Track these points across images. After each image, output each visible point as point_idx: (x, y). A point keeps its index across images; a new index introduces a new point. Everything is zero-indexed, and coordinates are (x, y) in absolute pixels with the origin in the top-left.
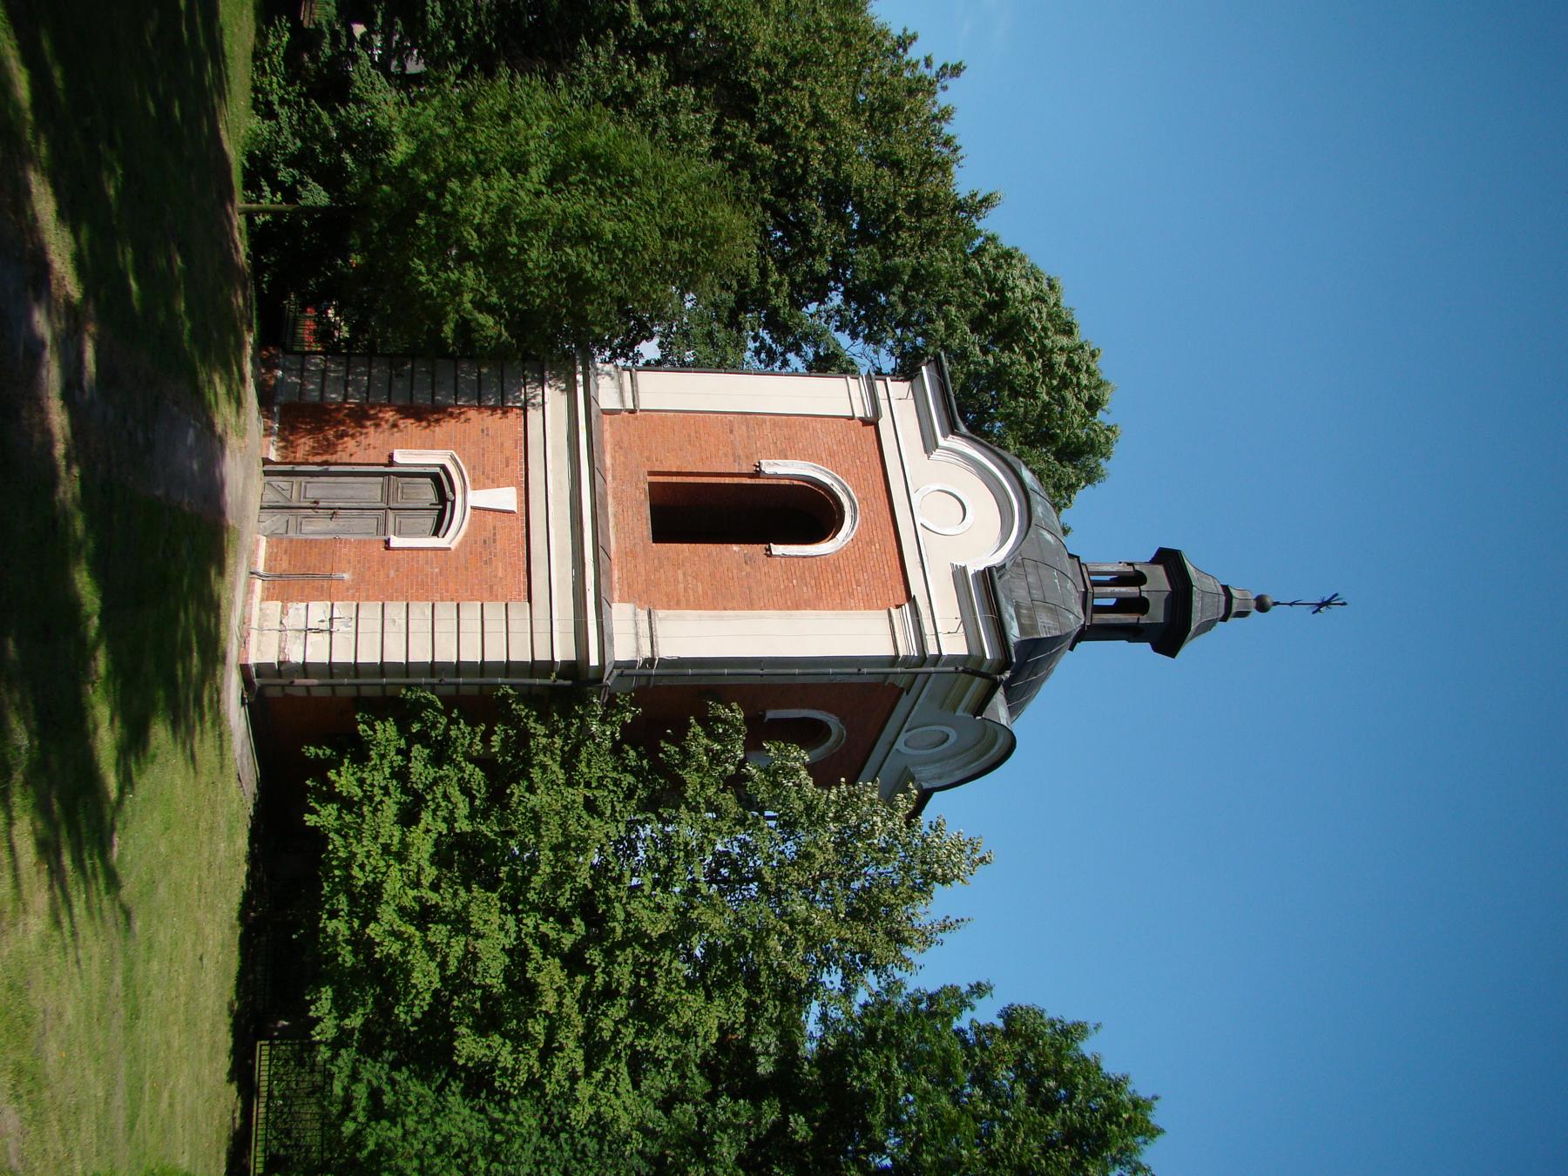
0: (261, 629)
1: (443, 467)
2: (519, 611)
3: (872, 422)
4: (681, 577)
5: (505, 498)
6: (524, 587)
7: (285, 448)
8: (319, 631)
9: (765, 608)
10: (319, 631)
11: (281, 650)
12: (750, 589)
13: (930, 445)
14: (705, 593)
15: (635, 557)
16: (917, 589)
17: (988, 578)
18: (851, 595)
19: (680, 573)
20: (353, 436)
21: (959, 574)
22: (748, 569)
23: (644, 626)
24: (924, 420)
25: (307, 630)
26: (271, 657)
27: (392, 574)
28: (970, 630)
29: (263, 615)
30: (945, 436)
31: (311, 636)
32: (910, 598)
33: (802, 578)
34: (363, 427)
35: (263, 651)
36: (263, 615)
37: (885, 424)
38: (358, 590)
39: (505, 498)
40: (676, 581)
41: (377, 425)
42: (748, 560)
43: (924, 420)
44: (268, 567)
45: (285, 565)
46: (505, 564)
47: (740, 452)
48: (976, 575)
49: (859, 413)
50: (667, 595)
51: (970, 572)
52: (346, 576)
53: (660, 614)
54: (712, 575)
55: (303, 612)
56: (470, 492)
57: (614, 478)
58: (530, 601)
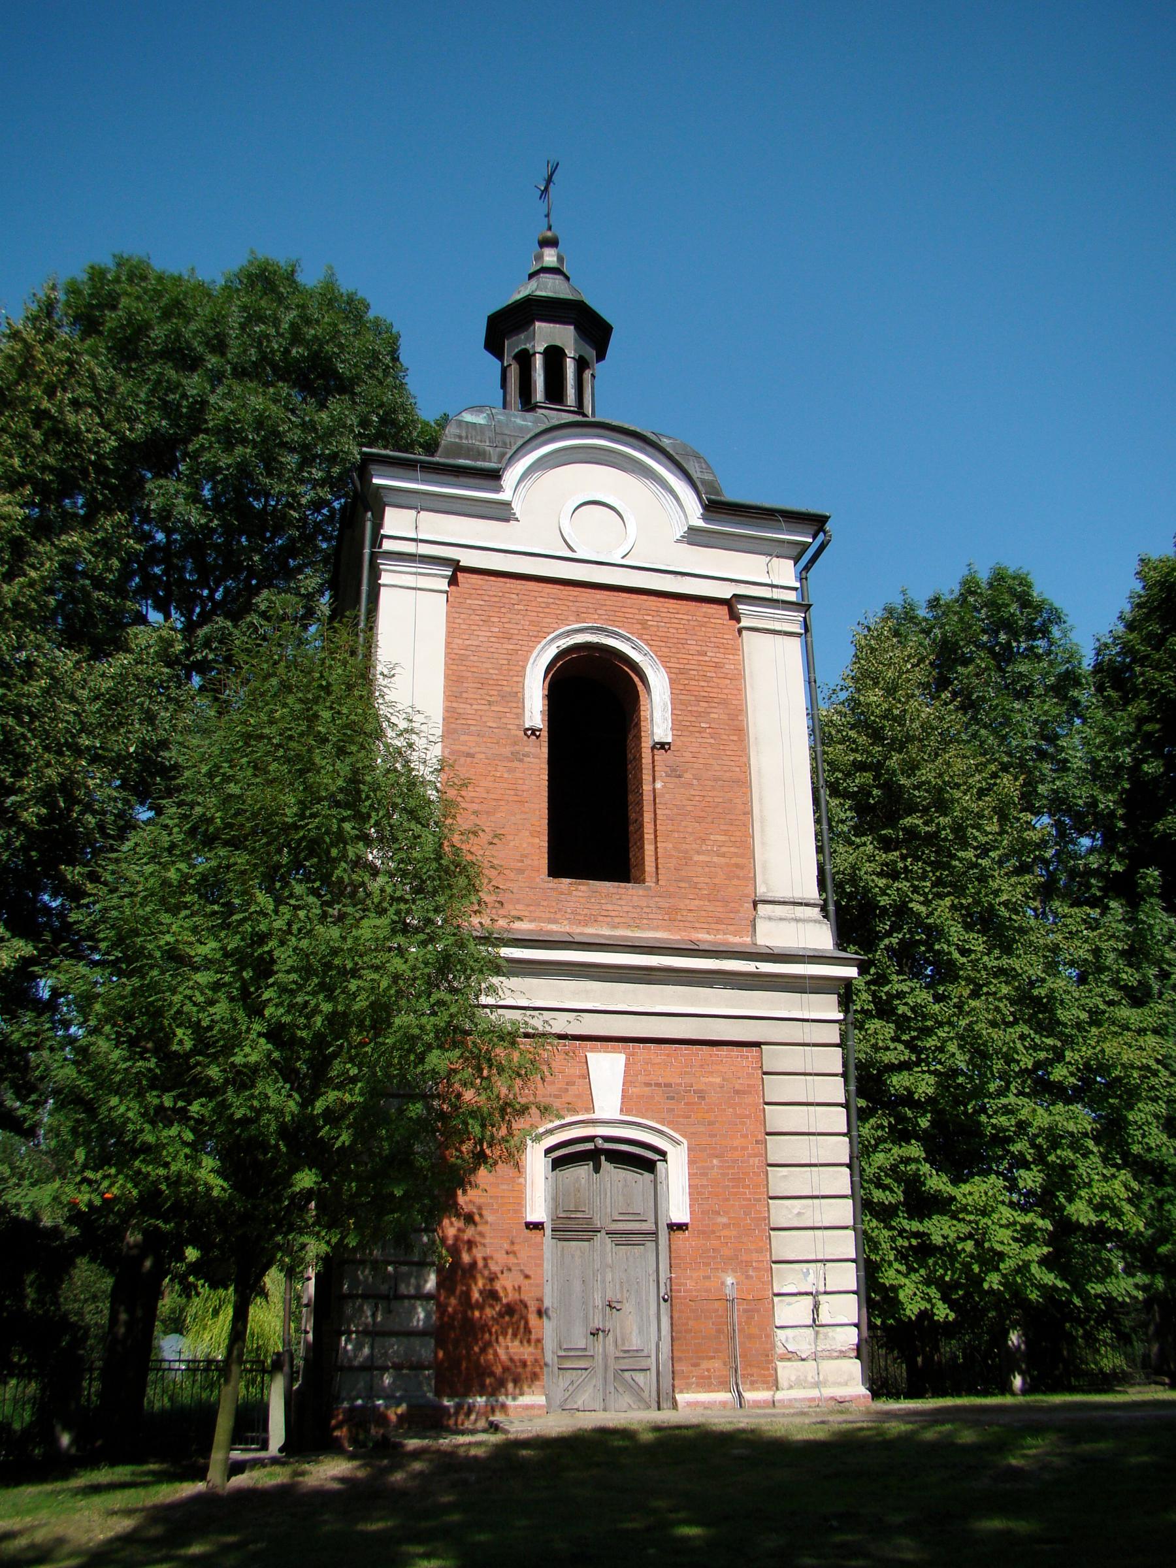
0: (817, 1385)
1: (548, 1151)
2: (774, 1058)
3: (457, 570)
4: (702, 858)
5: (607, 1072)
6: (735, 1051)
7: (516, 1381)
8: (816, 1307)
9: (748, 765)
10: (816, 1307)
11: (842, 1355)
12: (716, 780)
13: (502, 513)
14: (726, 833)
15: (677, 910)
16: (725, 591)
17: (714, 507)
18: (717, 666)
19: (696, 858)
20: (492, 1278)
21: (694, 537)
22: (688, 776)
23: (779, 910)
24: (467, 510)
25: (815, 1324)
26: (854, 1367)
27: (723, 1220)
28: (777, 551)
29: (799, 1383)
30: (499, 489)
31: (824, 1318)
32: (730, 605)
33: (699, 715)
34: (474, 1264)
35: (846, 1381)
36: (799, 1383)
37: (468, 559)
38: (748, 1264)
39: (607, 1072)
40: (707, 864)
41: (470, 1244)
42: (675, 773)
43: (457, 506)
44: (723, 1385)
45: (717, 1364)
46: (703, 1076)
47: (506, 751)
48: (705, 518)
49: (443, 584)
50: (729, 878)
51: (701, 523)
52: (729, 1280)
53: (762, 891)
54: (699, 819)
55: (788, 1331)
56: (598, 1115)
57: (555, 921)
58: (758, 1044)
